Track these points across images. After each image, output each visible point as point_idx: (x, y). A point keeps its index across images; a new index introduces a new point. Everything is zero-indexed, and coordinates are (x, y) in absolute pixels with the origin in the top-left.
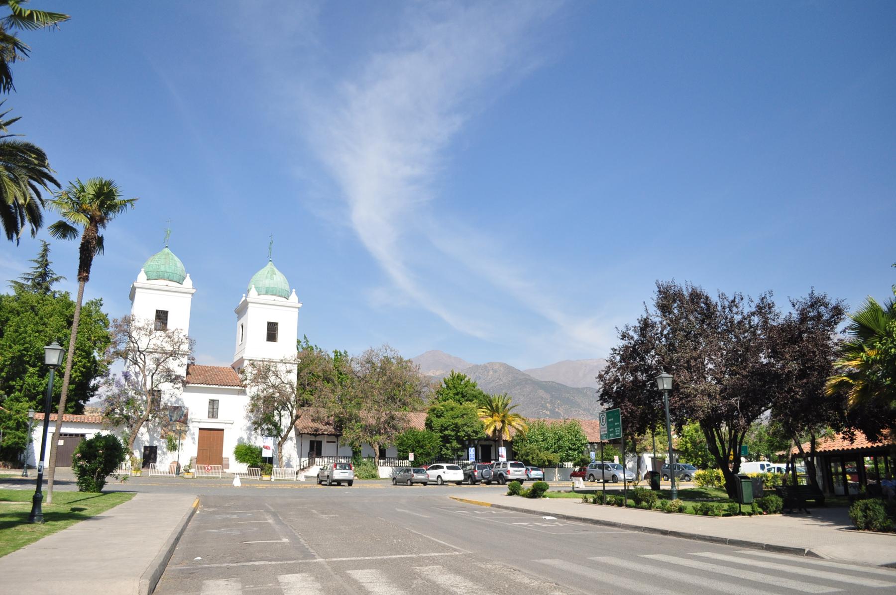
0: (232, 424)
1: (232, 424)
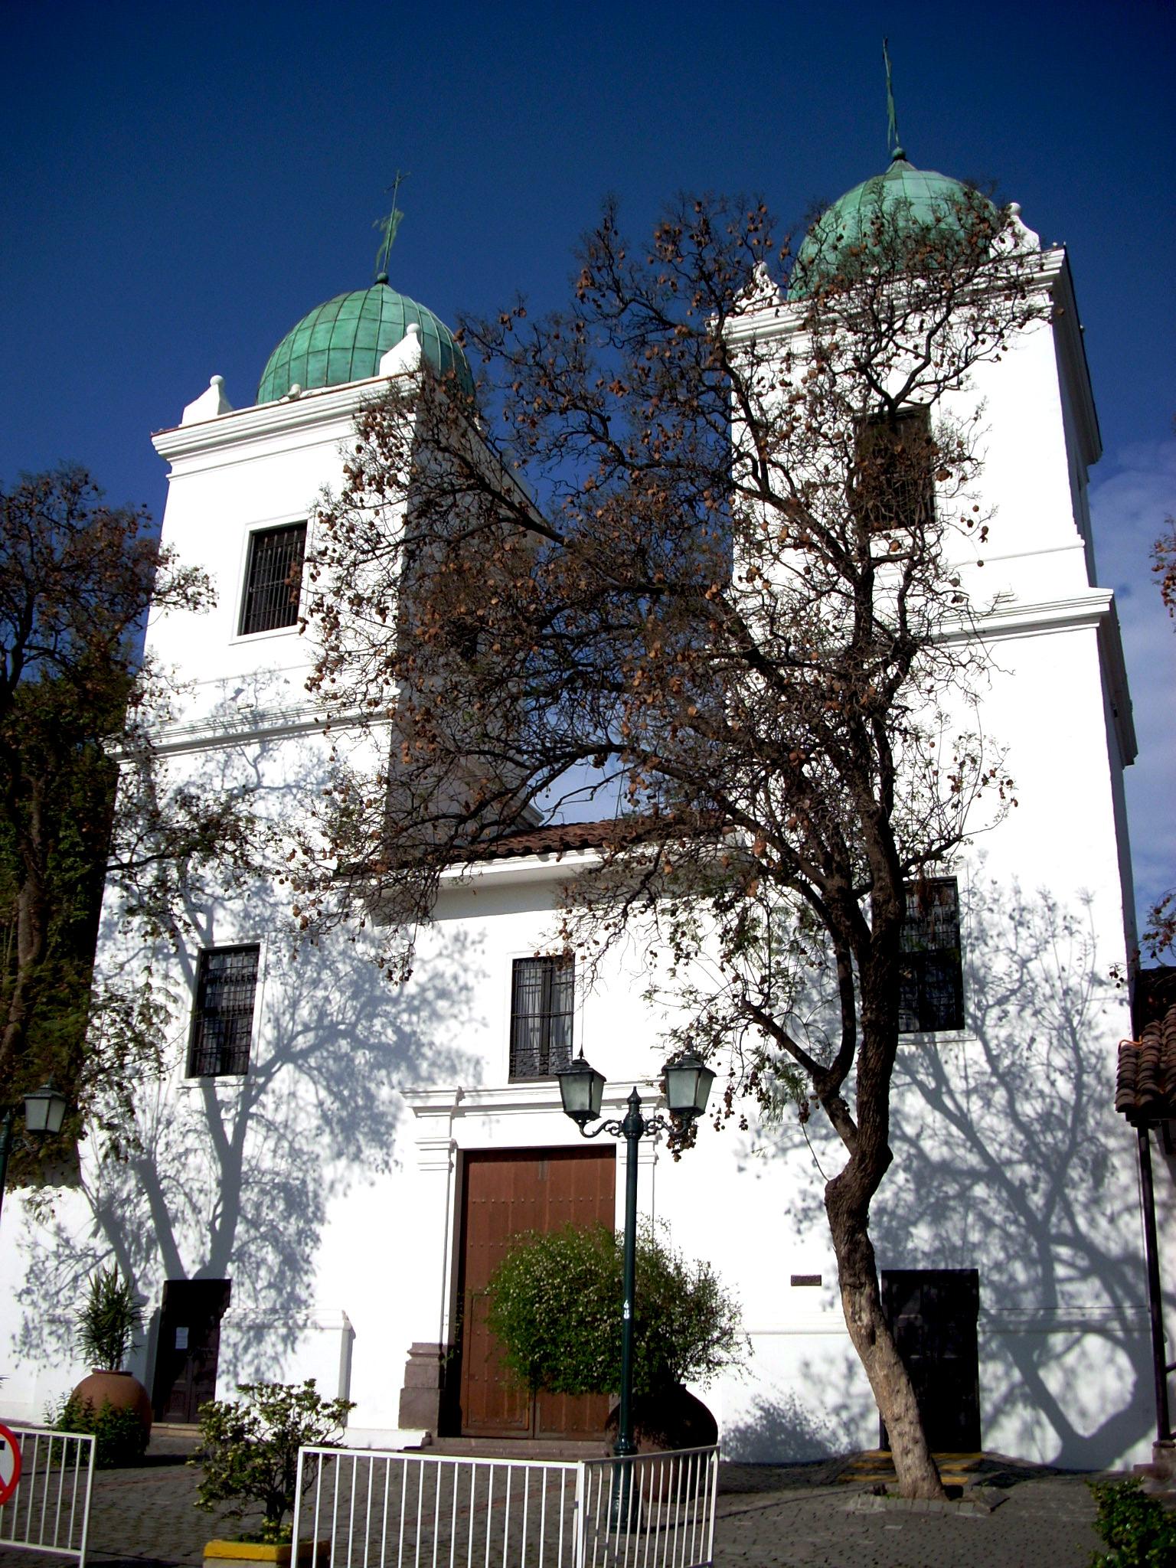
0: (350, 1334)
1: (350, 1334)
